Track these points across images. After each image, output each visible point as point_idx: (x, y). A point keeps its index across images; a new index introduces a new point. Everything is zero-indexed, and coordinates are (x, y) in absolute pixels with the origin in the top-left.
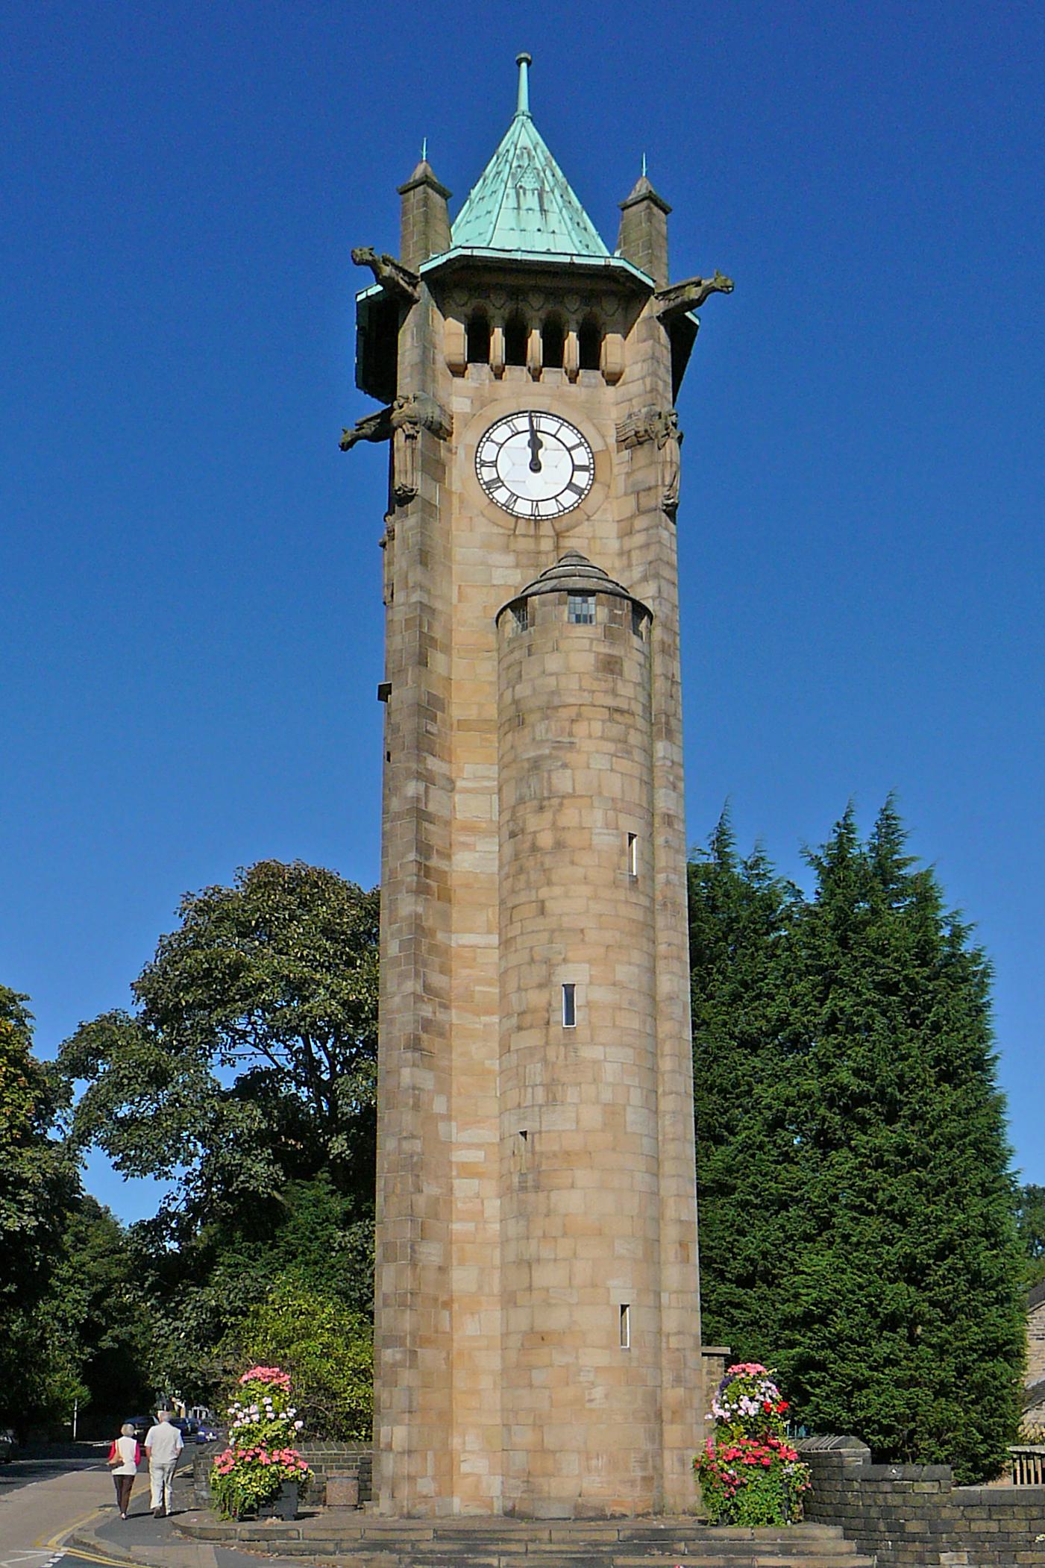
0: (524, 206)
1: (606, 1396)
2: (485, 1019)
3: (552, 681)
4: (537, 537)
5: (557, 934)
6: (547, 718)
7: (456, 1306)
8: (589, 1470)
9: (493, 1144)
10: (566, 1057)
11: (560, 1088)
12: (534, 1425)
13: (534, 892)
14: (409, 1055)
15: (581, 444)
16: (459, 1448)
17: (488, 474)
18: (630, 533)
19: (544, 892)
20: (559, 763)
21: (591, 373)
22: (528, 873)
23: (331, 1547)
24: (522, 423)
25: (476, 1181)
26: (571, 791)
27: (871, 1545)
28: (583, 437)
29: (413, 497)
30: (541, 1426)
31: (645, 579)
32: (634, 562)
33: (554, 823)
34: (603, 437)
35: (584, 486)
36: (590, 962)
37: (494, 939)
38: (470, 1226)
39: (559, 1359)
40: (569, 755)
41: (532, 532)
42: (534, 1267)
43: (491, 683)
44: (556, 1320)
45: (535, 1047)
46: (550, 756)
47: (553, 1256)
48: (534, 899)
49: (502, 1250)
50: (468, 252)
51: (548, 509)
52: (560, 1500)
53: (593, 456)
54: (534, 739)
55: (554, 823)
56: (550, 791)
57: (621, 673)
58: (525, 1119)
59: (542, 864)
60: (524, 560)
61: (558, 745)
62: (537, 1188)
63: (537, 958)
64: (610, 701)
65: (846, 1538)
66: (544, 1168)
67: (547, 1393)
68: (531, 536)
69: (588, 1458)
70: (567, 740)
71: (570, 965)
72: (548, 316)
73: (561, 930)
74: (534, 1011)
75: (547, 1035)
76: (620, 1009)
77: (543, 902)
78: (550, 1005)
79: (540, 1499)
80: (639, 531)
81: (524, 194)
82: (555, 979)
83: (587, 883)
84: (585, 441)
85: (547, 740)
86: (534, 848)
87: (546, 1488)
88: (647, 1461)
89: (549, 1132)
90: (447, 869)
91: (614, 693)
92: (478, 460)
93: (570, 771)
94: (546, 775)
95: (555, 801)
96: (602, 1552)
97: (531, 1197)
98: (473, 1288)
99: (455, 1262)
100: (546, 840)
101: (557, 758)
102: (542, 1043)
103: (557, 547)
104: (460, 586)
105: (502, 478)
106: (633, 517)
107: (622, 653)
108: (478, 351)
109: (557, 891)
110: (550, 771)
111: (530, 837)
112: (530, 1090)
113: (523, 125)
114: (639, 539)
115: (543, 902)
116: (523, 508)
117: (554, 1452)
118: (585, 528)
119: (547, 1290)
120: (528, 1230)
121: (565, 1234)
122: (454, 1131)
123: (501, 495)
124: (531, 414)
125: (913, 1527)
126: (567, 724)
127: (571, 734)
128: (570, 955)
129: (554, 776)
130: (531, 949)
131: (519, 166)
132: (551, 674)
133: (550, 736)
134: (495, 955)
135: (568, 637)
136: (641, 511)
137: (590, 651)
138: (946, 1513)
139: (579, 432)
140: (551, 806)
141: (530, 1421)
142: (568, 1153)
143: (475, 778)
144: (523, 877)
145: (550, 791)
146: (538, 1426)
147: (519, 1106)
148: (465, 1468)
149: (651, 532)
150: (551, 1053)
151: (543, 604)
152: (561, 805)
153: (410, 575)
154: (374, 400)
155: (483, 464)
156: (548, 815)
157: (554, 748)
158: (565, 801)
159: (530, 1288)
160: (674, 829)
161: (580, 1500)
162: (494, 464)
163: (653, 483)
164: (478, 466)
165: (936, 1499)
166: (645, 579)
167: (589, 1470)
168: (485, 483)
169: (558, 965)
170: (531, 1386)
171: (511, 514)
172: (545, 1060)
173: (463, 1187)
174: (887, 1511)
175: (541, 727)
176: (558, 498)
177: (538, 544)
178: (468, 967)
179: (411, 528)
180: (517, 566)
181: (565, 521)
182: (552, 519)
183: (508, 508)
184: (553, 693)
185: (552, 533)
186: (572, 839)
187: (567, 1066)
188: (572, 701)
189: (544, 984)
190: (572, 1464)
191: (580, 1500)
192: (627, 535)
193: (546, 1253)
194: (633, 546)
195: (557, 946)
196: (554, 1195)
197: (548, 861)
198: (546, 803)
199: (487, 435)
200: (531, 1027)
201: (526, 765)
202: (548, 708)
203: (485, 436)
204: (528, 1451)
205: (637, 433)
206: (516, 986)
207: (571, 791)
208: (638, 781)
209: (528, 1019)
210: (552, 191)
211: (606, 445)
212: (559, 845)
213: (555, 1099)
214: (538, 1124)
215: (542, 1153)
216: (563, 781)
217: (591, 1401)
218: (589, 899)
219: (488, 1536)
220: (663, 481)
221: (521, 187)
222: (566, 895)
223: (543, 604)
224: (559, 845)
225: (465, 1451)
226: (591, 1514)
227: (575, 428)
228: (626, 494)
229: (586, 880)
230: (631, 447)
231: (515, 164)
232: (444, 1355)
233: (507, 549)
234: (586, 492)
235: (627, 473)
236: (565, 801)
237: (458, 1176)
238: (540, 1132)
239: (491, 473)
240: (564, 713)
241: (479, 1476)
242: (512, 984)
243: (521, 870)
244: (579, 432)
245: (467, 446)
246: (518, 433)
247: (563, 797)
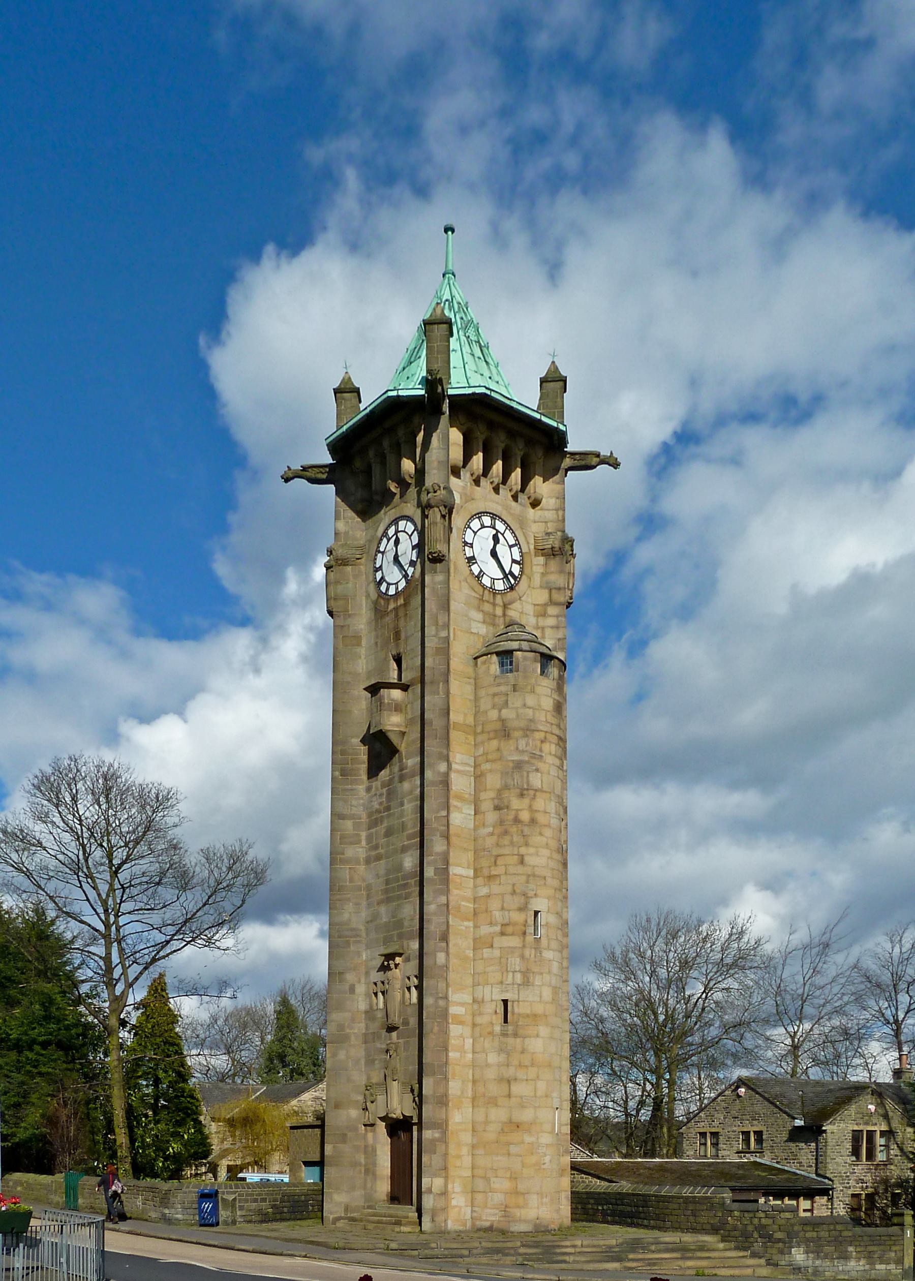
1: (550, 1161)
2: (466, 923)
3: (530, 712)
5: (531, 878)
6: (527, 736)
8: (542, 1204)
9: (469, 1004)
10: (535, 956)
12: (511, 1178)
13: (516, 849)
18: (544, 615)
19: (523, 850)
20: (534, 768)
22: (512, 836)
23: (466, 1252)
25: (460, 1027)
26: (540, 787)
27: (747, 1244)
29: (443, 560)
30: (516, 1178)
33: (530, 806)
34: (528, 543)
36: (549, 898)
37: (471, 873)
38: (457, 1055)
39: (528, 1139)
40: (540, 764)
41: (492, 600)
42: (512, 1083)
43: (470, 700)
44: (526, 1115)
45: (515, 948)
46: (528, 762)
47: (525, 1078)
48: (516, 853)
49: (473, 1070)
50: (488, 392)
52: (525, 1221)
54: (517, 748)
55: (530, 806)
56: (528, 785)
58: (507, 991)
59: (522, 832)
60: (488, 620)
61: (533, 756)
62: (516, 1035)
63: (518, 891)
65: (722, 1241)
66: (520, 1023)
67: (520, 1158)
69: (542, 1198)
70: (538, 753)
71: (538, 899)
73: (534, 875)
74: (515, 924)
75: (524, 941)
77: (522, 856)
78: (526, 921)
79: (514, 1221)
80: (550, 616)
82: (529, 906)
83: (547, 848)
85: (526, 751)
86: (517, 820)
87: (519, 1215)
89: (524, 1001)
93: (539, 774)
94: (525, 774)
95: (532, 792)
96: (614, 1252)
97: (511, 1040)
98: (459, 1093)
100: (525, 816)
101: (533, 764)
102: (520, 945)
104: (454, 629)
105: (476, 556)
106: (546, 605)
109: (532, 850)
110: (528, 772)
111: (513, 812)
112: (511, 974)
115: (522, 856)
117: (523, 1194)
119: (521, 1097)
120: (508, 1059)
121: (532, 1065)
125: (778, 1235)
126: (539, 743)
127: (541, 750)
128: (539, 892)
129: (531, 775)
130: (514, 885)
132: (529, 708)
133: (528, 748)
134: (471, 883)
135: (539, 685)
136: (552, 602)
138: (796, 1228)
140: (528, 795)
141: (508, 1175)
142: (535, 1015)
144: (508, 838)
145: (528, 785)
147: (502, 983)
148: (454, 1203)
149: (560, 618)
150: (527, 952)
151: (525, 658)
152: (535, 795)
153: (440, 617)
154: (330, 456)
157: (531, 757)
158: (538, 794)
159: (509, 1096)
161: (538, 1221)
163: (562, 586)
165: (792, 1221)
167: (542, 1204)
169: (532, 897)
170: (509, 1154)
172: (522, 957)
173: (455, 1030)
174: (761, 1228)
175: (522, 744)
178: (457, 889)
179: (440, 583)
180: (484, 622)
184: (531, 720)
187: (535, 962)
189: (523, 909)
190: (533, 1200)
191: (538, 1221)
192: (542, 616)
193: (521, 1074)
194: (546, 624)
195: (531, 886)
196: (527, 1040)
197: (526, 830)
198: (525, 792)
200: (513, 934)
202: (527, 730)
205: (552, 548)
206: (500, 906)
207: (540, 787)
209: (510, 929)
211: (529, 550)
212: (533, 821)
213: (528, 982)
214: (517, 996)
215: (519, 1014)
217: (544, 1164)
219: (551, 1244)
220: (568, 586)
222: (537, 854)
223: (525, 658)
224: (533, 821)
225: (454, 1193)
226: (543, 1229)
228: (541, 587)
230: (545, 556)
233: (479, 609)
235: (542, 573)
236: (538, 794)
237: (453, 1024)
241: (461, 1207)
243: (506, 832)
244: (515, 536)
245: (458, 529)
247: (536, 790)
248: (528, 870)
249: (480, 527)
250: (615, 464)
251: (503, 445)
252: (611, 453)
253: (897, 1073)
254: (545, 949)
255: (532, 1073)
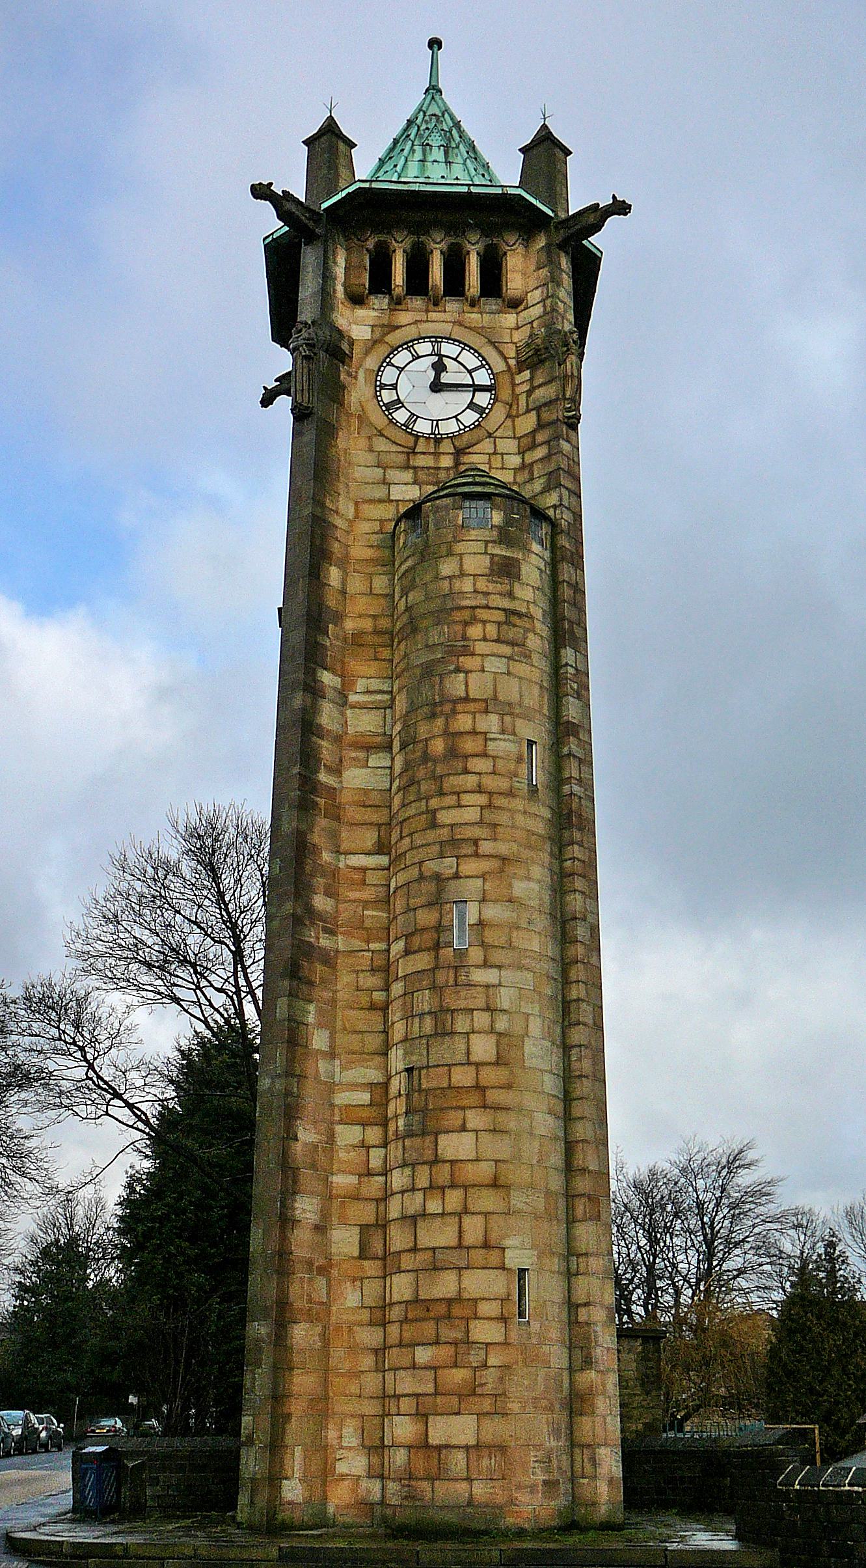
0: (430, 158)
4: (437, 454)
7: (334, 1272)
11: (449, 1016)
14: (286, 983)
15: (482, 366)
16: (335, 1442)
17: (387, 396)
18: (533, 446)
21: (492, 300)
24: (424, 348)
28: (484, 359)
31: (546, 490)
32: (536, 475)
34: (505, 359)
35: (485, 406)
51: (451, 427)
53: (495, 376)
57: (518, 577)
59: (434, 771)
64: (506, 603)
68: (430, 453)
72: (449, 248)
76: (518, 928)
81: (431, 150)
84: (485, 364)
86: (426, 758)
88: (550, 1461)
90: (336, 785)
91: (511, 595)
92: (378, 383)
95: (448, 708)
99: (335, 1221)
100: (438, 746)
103: (457, 464)
105: (402, 399)
107: (520, 556)
108: (380, 281)
112: (417, 1020)
113: (433, 98)
114: (540, 452)
116: (422, 427)
118: (487, 446)
121: (453, 1186)
122: (337, 1070)
123: (401, 416)
124: (437, 339)
131: (427, 129)
137: (486, 553)
139: (480, 355)
143: (369, 692)
145: (442, 695)
146: (422, 1416)
155: (383, 387)
156: (440, 722)
160: (579, 739)
162: (394, 387)
164: (378, 389)
166: (546, 490)
168: (384, 404)
171: (410, 433)
176: (458, 417)
177: (437, 460)
181: (466, 438)
182: (452, 437)
183: (408, 428)
185: (452, 451)
186: (469, 745)
188: (467, 603)
199: (388, 360)
201: (418, 671)
203: (386, 361)
204: (410, 1447)
208: (538, 687)
209: (416, 941)
210: (457, 147)
212: (453, 753)
216: (456, 686)
218: (482, 808)
220: (564, 395)
221: (428, 144)
224: (453, 753)
225: (342, 1448)
227: (476, 351)
229: (479, 790)
231: (423, 127)
232: (319, 1329)
234: (487, 411)
237: (341, 1122)
238: (428, 1067)
239: (391, 395)
240: (458, 616)
242: (399, 904)
246: (419, 357)
248: (444, 833)
249: (469, 368)
250: (620, 208)
251: (479, 247)
252: (614, 197)
253: (510, 885)
254: (477, 966)
255: (454, 1199)
